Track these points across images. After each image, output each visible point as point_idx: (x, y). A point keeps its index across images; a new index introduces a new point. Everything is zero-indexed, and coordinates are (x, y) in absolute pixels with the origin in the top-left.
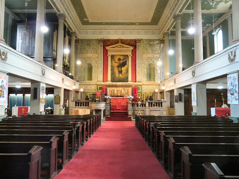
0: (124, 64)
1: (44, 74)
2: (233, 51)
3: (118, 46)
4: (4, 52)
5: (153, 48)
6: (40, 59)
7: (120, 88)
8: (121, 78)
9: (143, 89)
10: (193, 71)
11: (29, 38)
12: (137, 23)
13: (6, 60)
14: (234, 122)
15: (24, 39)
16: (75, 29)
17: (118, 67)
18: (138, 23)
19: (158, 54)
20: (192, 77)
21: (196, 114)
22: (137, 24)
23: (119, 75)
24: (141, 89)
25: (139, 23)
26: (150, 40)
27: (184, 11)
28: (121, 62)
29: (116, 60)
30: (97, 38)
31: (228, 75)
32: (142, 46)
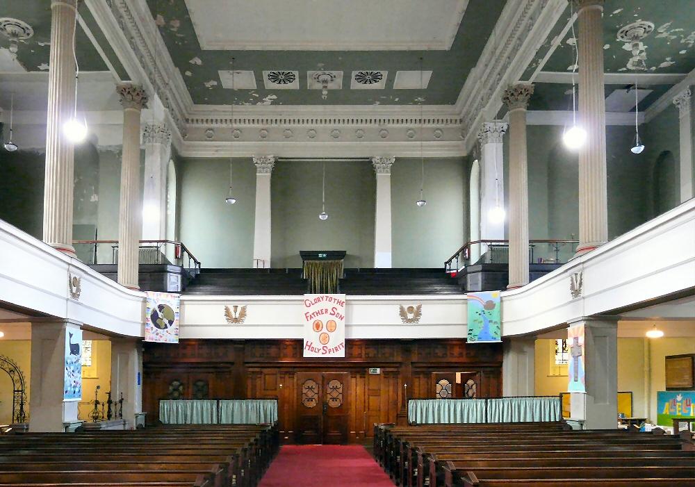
2: (579, 273)
16: (138, 72)
20: (571, 298)
27: (539, 75)
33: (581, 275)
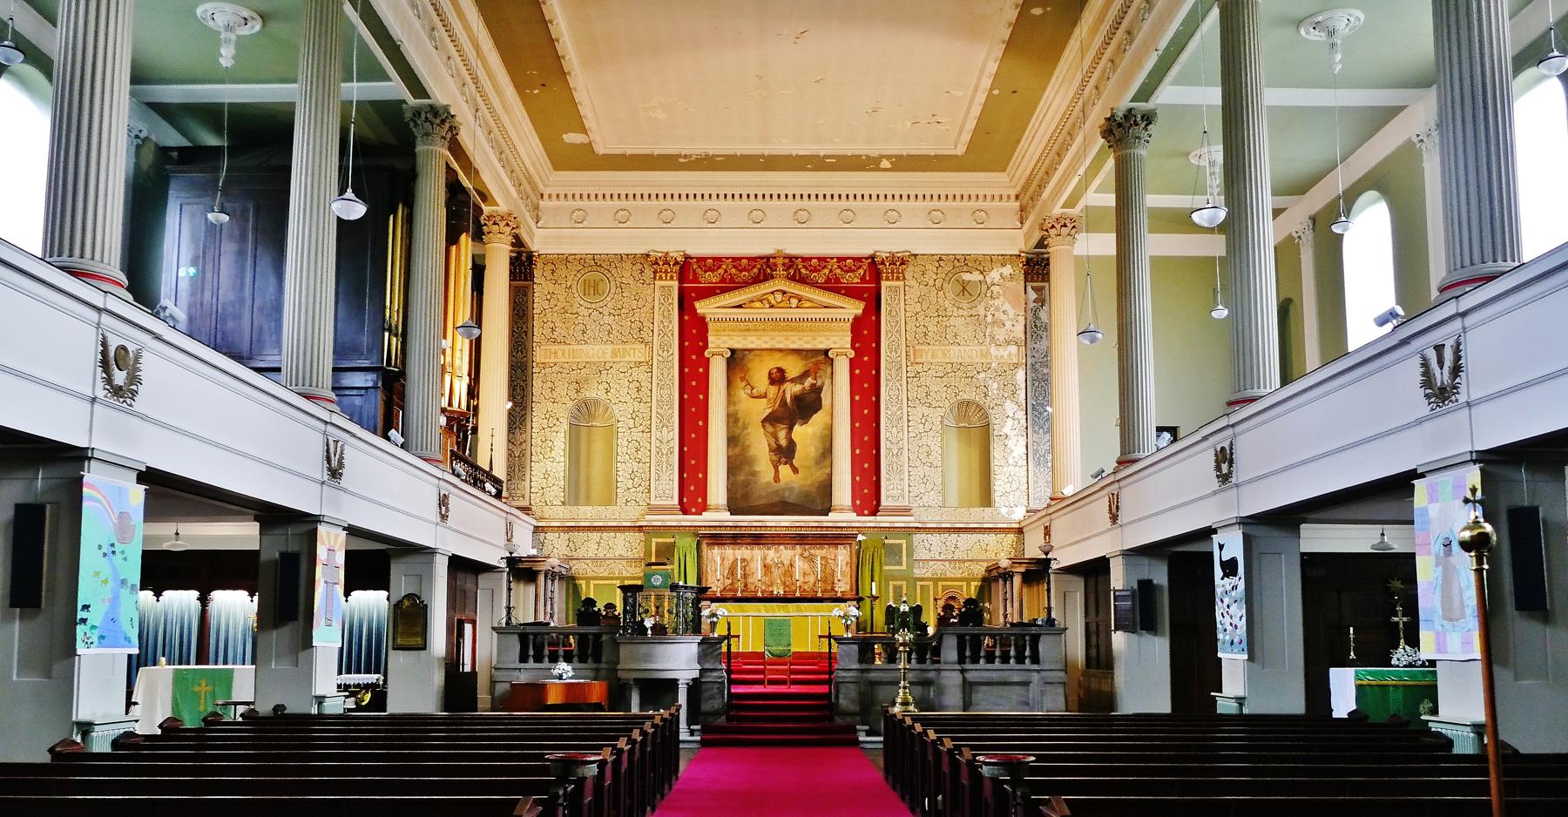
0: (806, 406)
1: (335, 474)
2: (1449, 344)
3: (771, 298)
4: (124, 348)
5: (981, 310)
6: (314, 384)
7: (782, 547)
8: (791, 489)
9: (921, 554)
10: (1223, 449)
11: (241, 253)
12: (882, 157)
13: (134, 393)
14: (1457, 750)
15: (205, 256)
17: (771, 420)
18: (888, 157)
19: (1008, 343)
20: (1215, 484)
21: (1241, 705)
22: (885, 164)
23: (777, 471)
24: (910, 553)
25: (899, 157)
26: (964, 262)
28: (791, 389)
29: (760, 379)
30: (640, 250)
31: (1422, 476)
32: (913, 294)
33: (1118, 496)
